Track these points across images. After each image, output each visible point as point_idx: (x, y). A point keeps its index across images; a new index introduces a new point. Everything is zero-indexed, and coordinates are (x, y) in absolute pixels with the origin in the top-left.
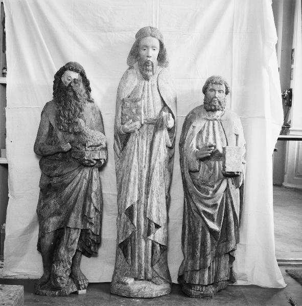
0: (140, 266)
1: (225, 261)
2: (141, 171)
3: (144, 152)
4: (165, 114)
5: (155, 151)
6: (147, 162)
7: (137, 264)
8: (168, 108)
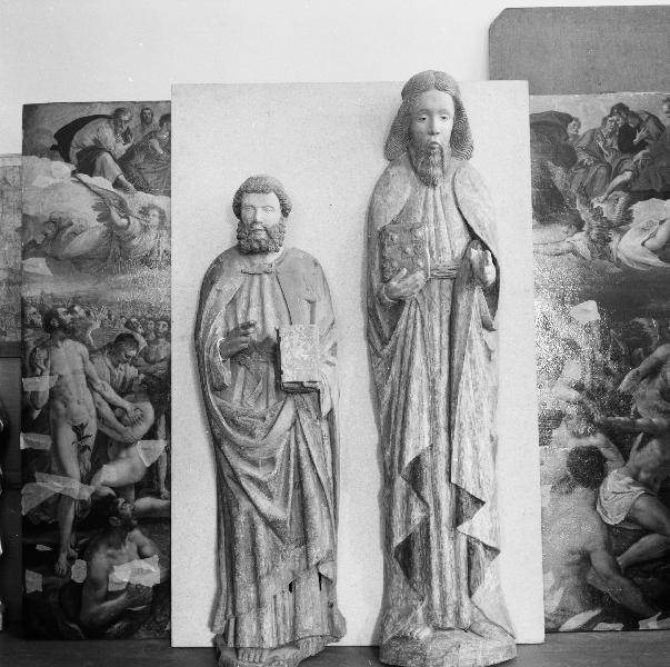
0: (444, 595)
1: (310, 588)
2: (434, 381)
3: (437, 338)
4: (475, 253)
5: (459, 335)
6: (446, 361)
7: (436, 593)
8: (482, 242)
